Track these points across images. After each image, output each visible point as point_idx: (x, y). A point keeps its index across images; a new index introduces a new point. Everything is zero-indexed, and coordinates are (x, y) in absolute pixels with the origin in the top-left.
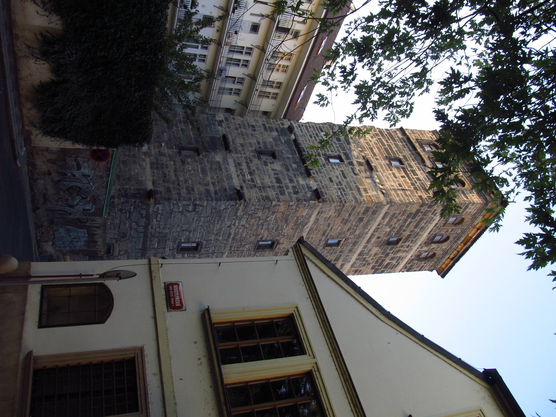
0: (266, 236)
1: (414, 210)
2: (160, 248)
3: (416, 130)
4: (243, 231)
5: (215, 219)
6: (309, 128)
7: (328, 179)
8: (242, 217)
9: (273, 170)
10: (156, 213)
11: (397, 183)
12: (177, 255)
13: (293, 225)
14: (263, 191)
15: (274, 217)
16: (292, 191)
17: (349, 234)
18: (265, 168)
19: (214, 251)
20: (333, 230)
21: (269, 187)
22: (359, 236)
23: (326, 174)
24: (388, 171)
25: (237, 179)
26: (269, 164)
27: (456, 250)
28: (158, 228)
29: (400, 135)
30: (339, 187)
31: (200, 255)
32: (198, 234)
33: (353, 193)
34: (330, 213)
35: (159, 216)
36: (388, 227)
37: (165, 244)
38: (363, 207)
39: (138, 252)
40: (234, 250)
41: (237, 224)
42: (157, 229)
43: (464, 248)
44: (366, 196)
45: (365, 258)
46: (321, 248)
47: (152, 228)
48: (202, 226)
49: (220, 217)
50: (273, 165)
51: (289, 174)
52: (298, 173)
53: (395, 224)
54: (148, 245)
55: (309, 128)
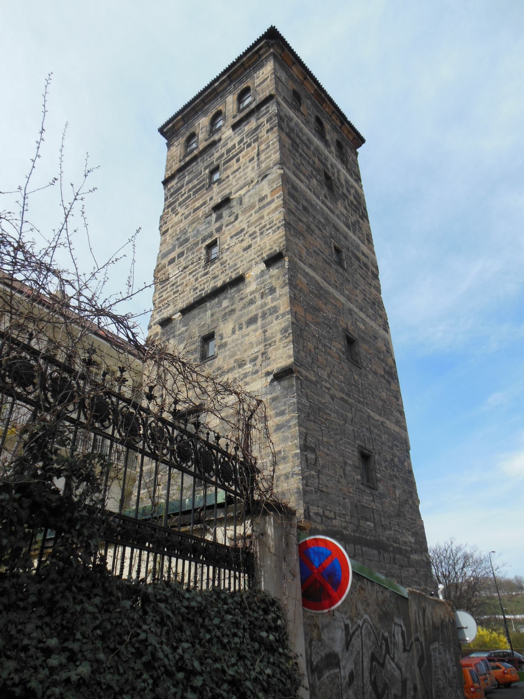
0: (340, 346)
1: (288, 142)
2: (374, 517)
3: (167, 166)
4: (336, 378)
5: (323, 418)
6: (162, 298)
7: (246, 252)
8: (317, 374)
9: (234, 332)
10: (324, 518)
11: (247, 165)
12: (379, 491)
13: (321, 302)
14: (273, 339)
15: (312, 326)
16: (271, 297)
17: (325, 231)
18: (231, 346)
19: (367, 429)
20: (323, 251)
21: (265, 332)
22: (327, 219)
23: (237, 257)
24: (229, 181)
25: (254, 384)
26: (223, 341)
27: (331, 116)
28: (344, 518)
29: (174, 183)
30: (258, 234)
31: (376, 453)
32: (347, 450)
33: (268, 214)
34: (301, 245)
35: (327, 513)
36: (311, 180)
37: (368, 508)
38: (289, 200)
39: (384, 557)
40: (364, 399)
41: (328, 385)
42: (347, 520)
43: (328, 102)
44: (272, 196)
45: (352, 223)
46: (346, 275)
47: (346, 528)
48: (336, 442)
49: (320, 409)
50: (224, 335)
51: (240, 308)
52: (238, 296)
53: (308, 171)
54: (372, 538)
55: (162, 298)
